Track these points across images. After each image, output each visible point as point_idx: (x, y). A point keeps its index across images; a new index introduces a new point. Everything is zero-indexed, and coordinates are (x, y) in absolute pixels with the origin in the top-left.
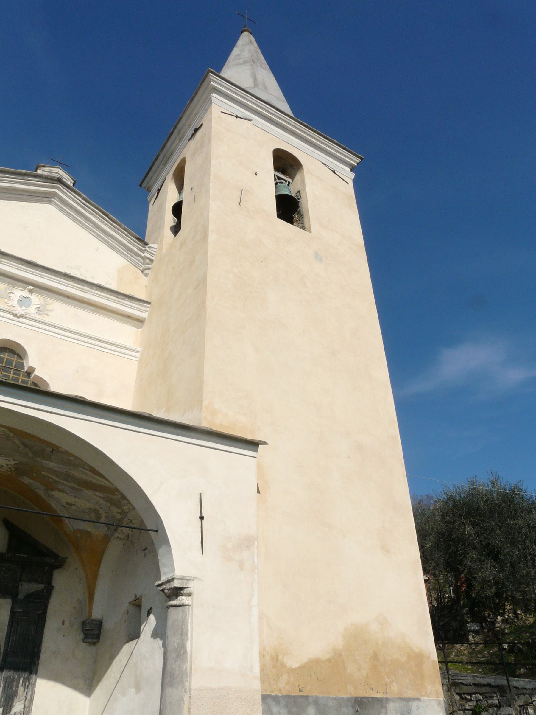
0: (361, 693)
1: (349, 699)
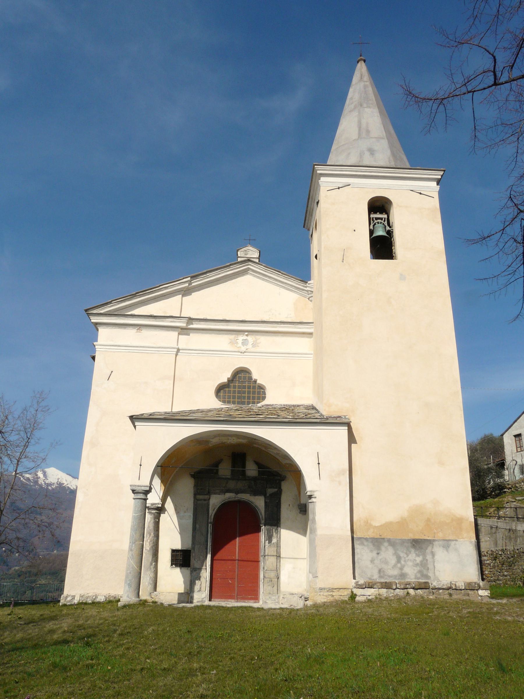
0: (417, 537)
1: (408, 540)
